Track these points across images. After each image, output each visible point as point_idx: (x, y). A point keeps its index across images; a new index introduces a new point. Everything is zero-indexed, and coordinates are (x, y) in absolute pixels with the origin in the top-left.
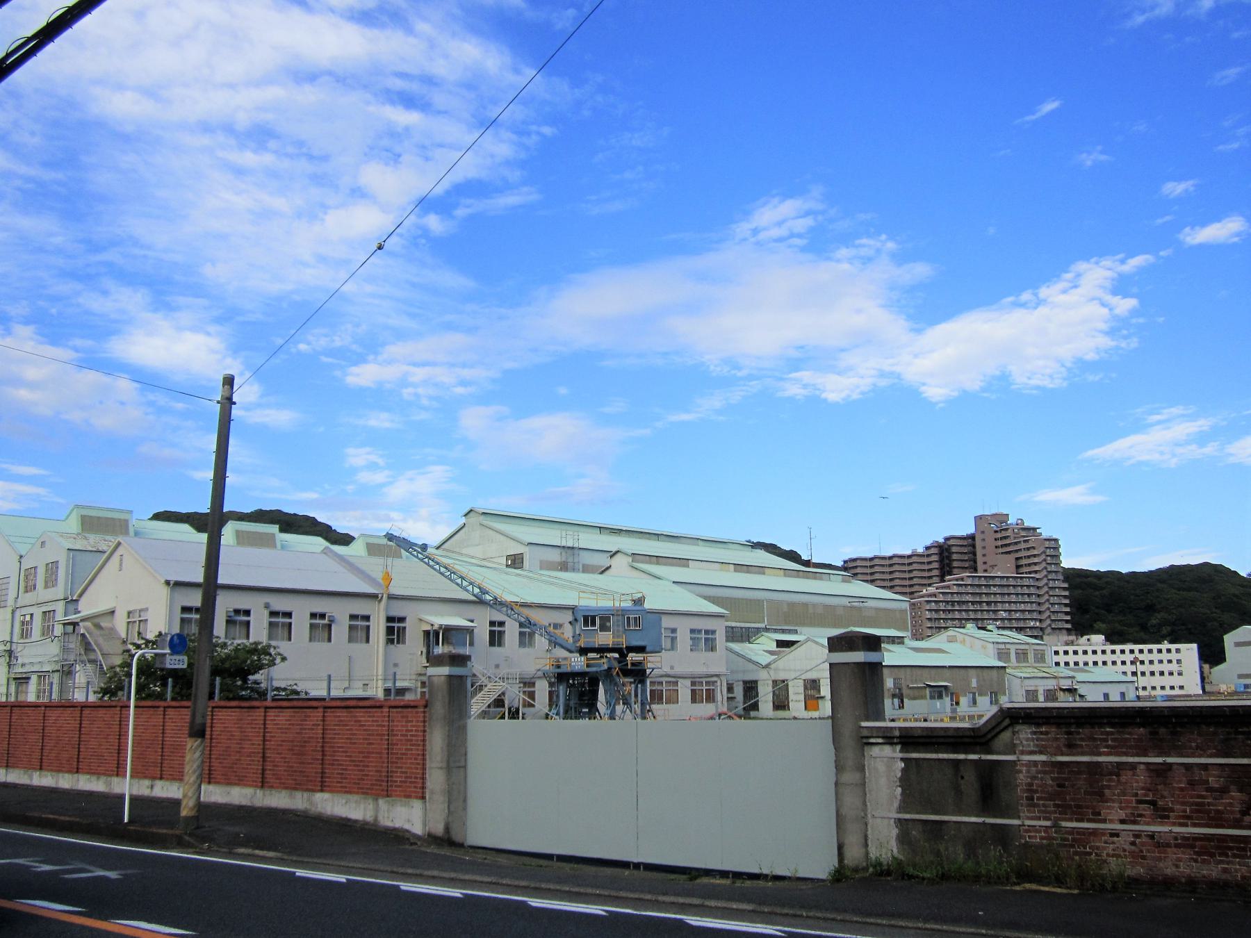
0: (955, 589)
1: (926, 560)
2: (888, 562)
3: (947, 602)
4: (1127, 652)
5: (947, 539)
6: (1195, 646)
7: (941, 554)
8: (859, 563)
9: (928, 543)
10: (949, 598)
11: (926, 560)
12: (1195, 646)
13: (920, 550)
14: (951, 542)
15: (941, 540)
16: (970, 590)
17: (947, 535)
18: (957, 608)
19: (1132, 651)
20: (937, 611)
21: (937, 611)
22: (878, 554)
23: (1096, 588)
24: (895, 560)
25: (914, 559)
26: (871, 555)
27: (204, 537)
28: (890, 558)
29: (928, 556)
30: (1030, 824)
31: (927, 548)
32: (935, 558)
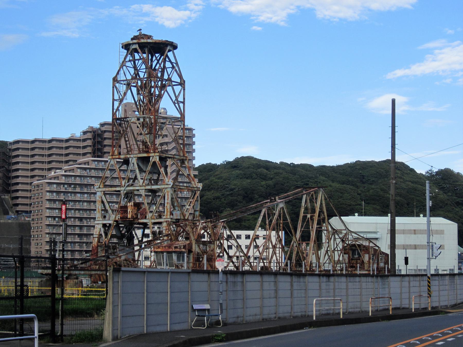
0: (78, 173)
1: (82, 144)
2: (47, 145)
3: (70, 185)
4: (243, 237)
5: (102, 125)
6: (396, 218)
7: (94, 138)
8: (20, 145)
9: (85, 128)
10: (71, 180)
11: (82, 144)
12: (396, 218)
13: (78, 135)
14: (103, 129)
15: (96, 125)
16: (93, 173)
17: (102, 121)
18: (78, 190)
19: (248, 237)
20: (58, 193)
21: (58, 193)
22: (40, 137)
23: (264, 178)
24: (54, 144)
25: (71, 143)
26: (31, 138)
27: (168, 160)
28: (50, 141)
29: (84, 140)
30: (350, 272)
31: (85, 133)
32: (89, 143)
